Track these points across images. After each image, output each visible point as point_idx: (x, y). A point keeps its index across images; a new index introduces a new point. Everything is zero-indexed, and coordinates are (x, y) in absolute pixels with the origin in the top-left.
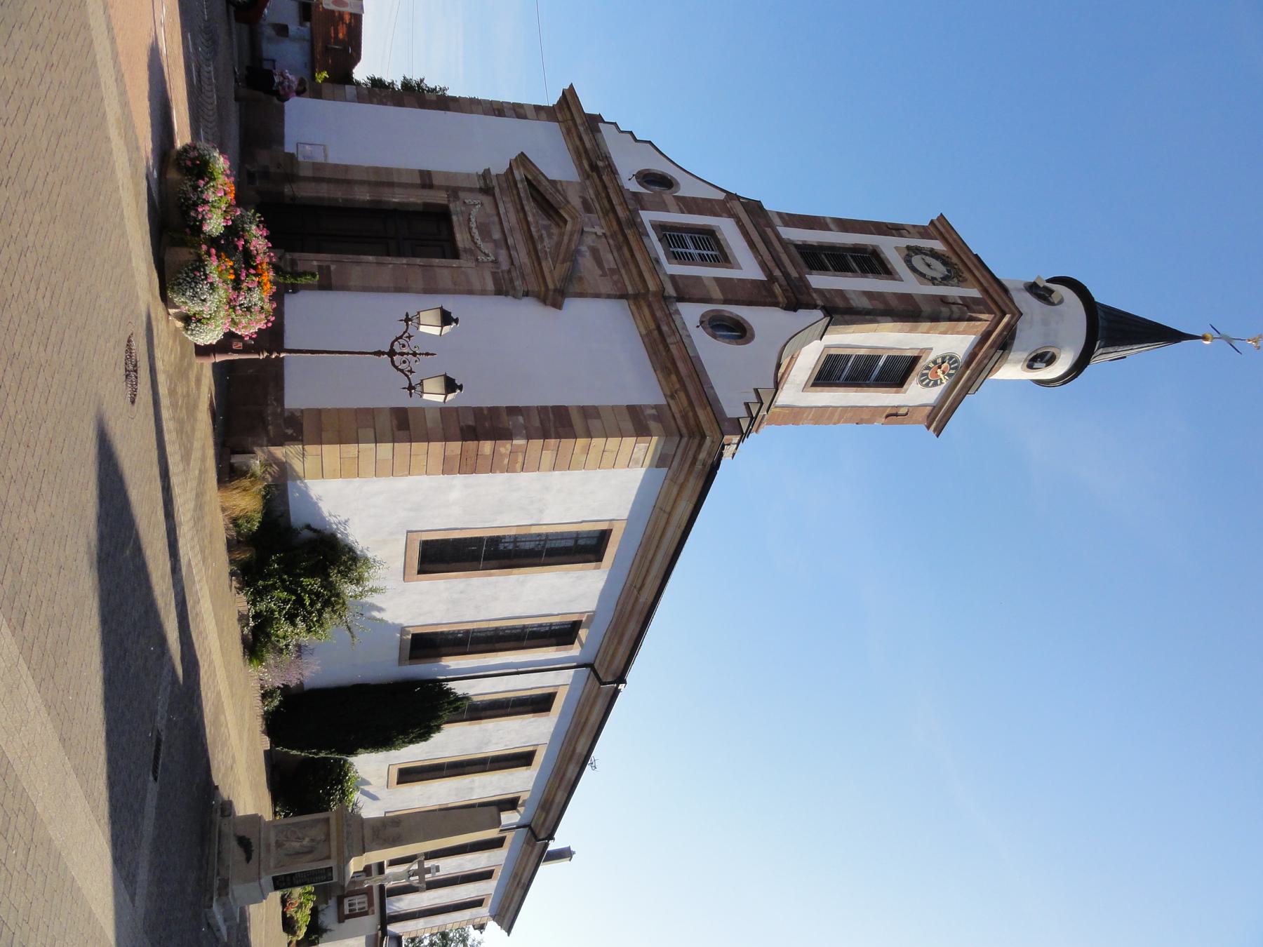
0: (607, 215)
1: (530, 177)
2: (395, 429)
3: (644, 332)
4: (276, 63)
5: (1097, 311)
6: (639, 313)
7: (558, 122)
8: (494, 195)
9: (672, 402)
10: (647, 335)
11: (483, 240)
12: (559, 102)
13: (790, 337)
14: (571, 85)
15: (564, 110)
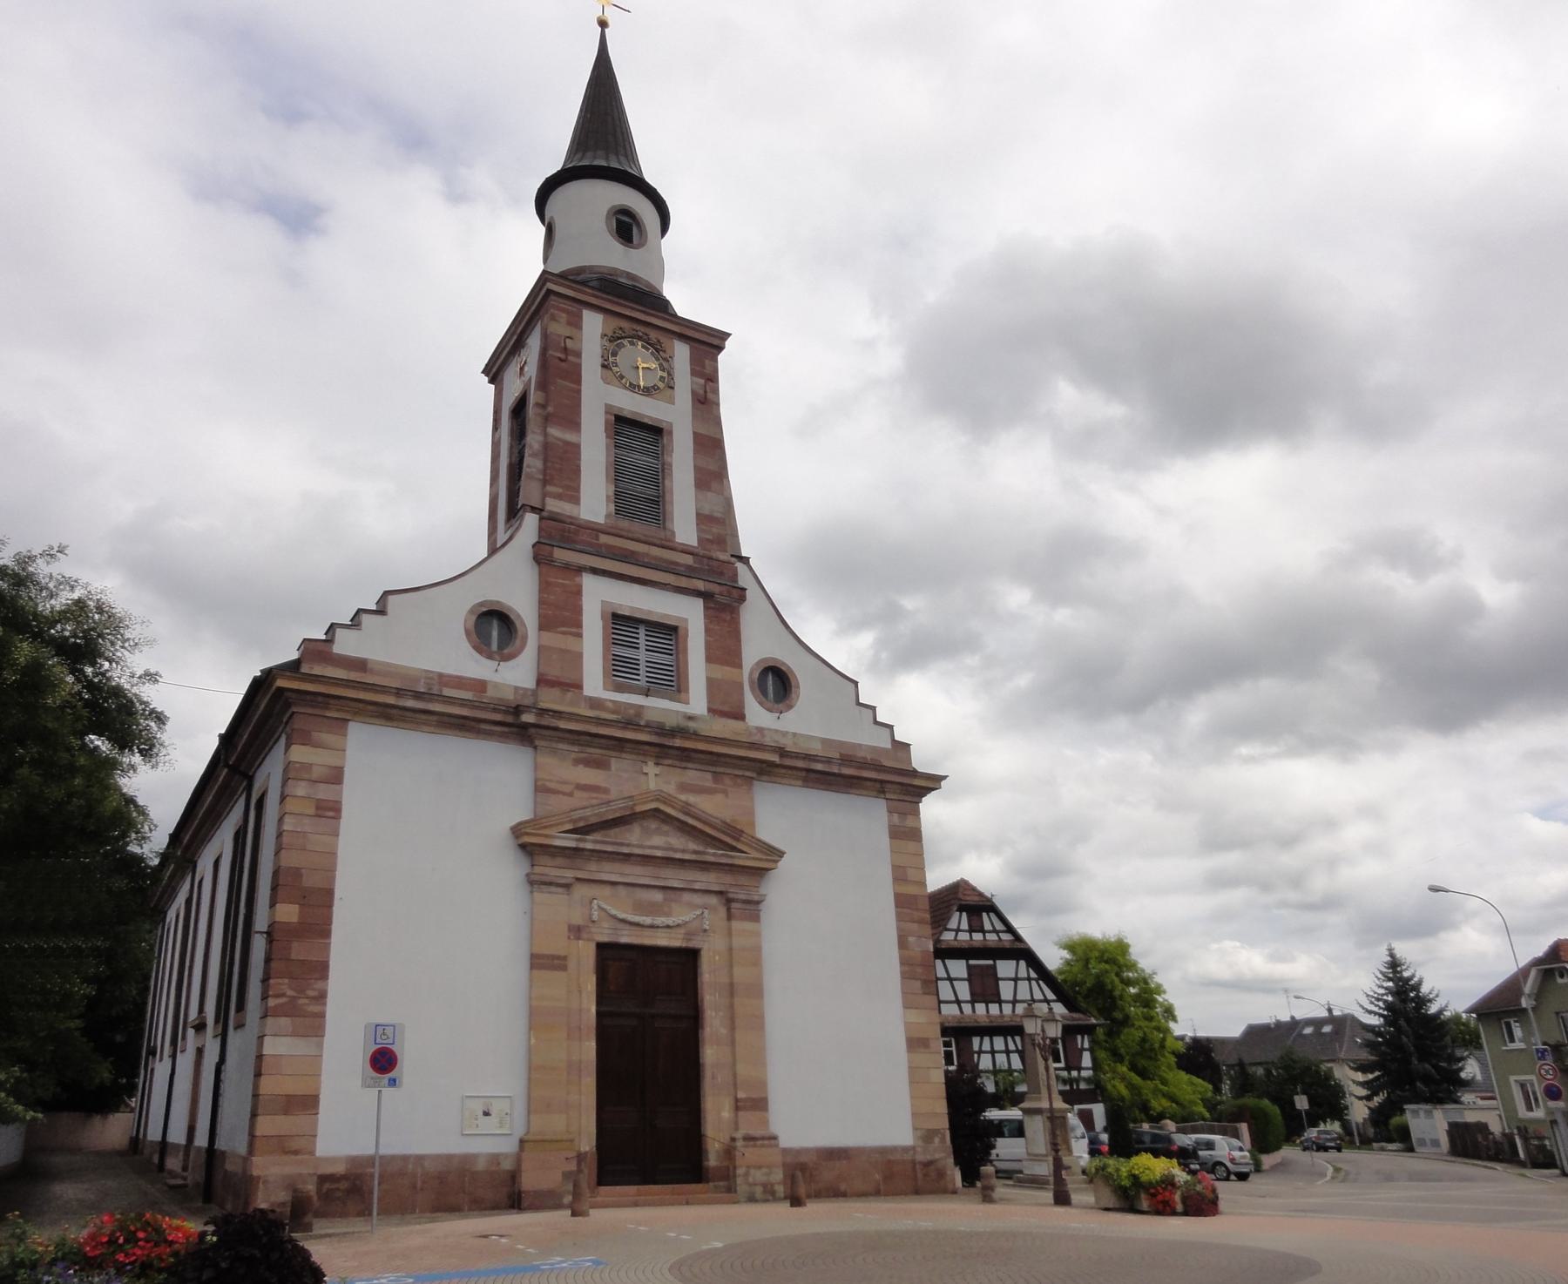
1: (569, 827)
3: (800, 783)
7: (349, 720)
8: (578, 879)
11: (668, 915)
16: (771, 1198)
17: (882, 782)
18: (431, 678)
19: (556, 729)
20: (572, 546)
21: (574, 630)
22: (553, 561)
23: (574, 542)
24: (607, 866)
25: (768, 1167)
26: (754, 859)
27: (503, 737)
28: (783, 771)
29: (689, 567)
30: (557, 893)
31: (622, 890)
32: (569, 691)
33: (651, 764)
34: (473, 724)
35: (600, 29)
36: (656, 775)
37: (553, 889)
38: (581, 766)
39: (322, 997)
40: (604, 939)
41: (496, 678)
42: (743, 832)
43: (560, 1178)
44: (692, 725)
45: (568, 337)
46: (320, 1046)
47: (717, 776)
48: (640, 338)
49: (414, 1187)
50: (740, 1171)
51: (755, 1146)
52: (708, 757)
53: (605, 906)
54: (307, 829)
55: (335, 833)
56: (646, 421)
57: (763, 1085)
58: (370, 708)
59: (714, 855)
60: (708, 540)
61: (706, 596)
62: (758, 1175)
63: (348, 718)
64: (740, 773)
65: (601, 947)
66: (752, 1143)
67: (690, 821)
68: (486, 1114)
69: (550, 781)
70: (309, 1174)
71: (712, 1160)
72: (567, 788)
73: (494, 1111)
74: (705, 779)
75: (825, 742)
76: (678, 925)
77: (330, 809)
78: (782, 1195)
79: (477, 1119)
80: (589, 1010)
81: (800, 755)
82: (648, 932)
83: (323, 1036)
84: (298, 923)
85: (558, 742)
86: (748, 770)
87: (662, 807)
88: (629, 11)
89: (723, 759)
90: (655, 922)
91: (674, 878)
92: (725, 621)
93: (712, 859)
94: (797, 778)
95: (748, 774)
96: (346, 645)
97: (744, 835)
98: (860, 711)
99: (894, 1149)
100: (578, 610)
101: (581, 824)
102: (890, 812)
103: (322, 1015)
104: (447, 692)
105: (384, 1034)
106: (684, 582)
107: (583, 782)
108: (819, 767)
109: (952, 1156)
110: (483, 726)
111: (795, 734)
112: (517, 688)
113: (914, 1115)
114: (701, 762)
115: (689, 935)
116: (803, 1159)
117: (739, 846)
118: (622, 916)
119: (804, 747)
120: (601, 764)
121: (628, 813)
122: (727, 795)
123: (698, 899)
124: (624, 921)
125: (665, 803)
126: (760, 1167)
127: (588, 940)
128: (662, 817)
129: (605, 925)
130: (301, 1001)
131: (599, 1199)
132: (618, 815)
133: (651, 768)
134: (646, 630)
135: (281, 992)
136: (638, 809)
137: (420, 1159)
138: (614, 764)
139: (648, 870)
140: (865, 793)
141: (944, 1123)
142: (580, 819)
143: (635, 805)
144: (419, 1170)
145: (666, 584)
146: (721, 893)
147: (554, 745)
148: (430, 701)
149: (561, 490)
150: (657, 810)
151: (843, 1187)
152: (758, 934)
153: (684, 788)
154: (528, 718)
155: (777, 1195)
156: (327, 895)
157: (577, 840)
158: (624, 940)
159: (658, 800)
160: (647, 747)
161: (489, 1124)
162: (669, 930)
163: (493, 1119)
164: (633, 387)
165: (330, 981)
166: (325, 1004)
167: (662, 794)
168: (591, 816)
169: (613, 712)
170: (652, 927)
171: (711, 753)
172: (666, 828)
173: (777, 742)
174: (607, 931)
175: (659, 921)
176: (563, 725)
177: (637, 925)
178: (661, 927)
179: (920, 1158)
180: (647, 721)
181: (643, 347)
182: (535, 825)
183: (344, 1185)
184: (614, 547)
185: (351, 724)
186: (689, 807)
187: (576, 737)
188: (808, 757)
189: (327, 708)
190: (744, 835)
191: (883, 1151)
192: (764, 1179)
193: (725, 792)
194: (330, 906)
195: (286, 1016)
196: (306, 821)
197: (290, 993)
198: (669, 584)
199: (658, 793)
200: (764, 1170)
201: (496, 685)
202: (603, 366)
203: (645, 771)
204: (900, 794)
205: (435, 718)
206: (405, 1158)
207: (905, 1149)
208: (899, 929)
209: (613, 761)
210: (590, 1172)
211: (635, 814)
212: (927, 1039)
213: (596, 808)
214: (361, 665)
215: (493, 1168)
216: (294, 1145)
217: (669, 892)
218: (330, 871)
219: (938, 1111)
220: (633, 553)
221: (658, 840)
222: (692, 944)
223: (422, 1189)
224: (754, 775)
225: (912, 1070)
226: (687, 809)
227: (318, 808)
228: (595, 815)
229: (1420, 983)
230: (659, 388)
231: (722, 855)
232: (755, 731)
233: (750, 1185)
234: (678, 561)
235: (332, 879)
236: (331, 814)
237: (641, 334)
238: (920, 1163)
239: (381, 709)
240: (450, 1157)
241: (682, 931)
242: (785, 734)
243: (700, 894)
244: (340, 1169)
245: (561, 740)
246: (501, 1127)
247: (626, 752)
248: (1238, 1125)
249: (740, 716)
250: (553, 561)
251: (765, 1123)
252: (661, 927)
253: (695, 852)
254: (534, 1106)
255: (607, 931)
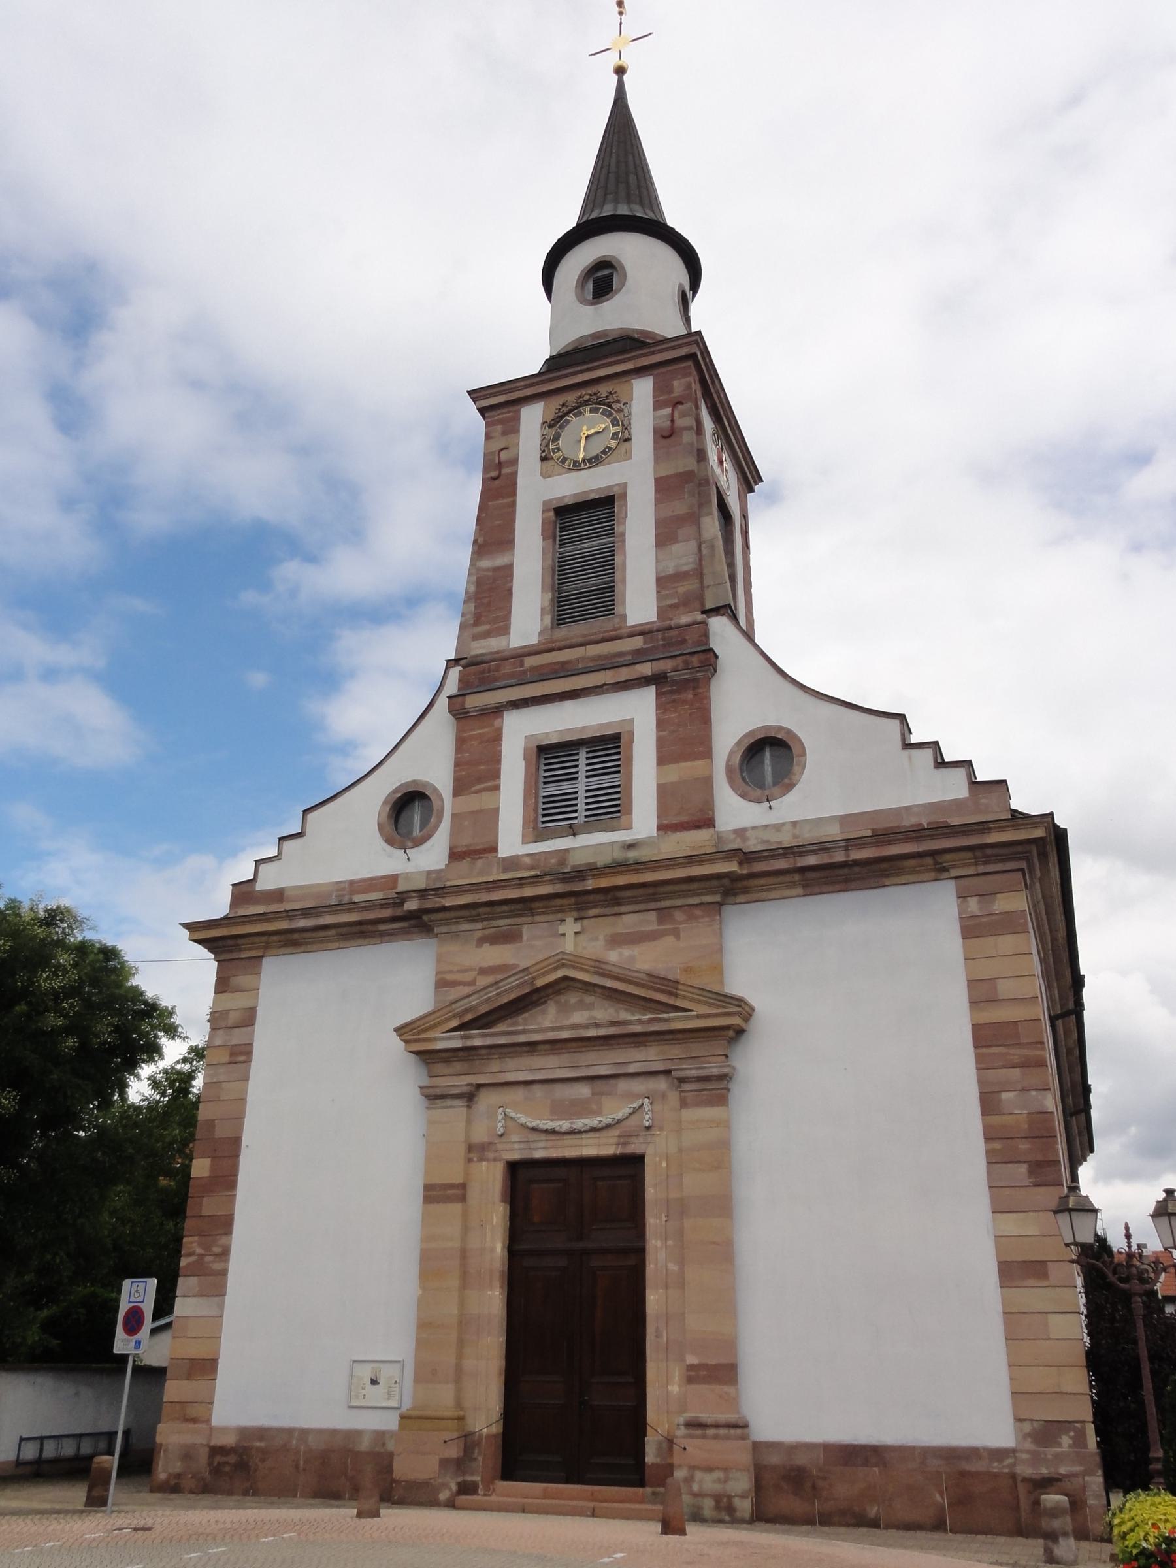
0: (531, 909)
1: (455, 1023)
2: (1046, 1283)
3: (800, 891)
4: (24, 1437)
5: (592, 219)
6: (758, 891)
7: (262, 957)
8: (479, 1086)
9: (954, 873)
10: (804, 886)
11: (598, 1113)
12: (211, 950)
13: (778, 677)
14: (187, 926)
15: (238, 945)
16: (727, 1518)
17: (933, 854)
18: (343, 889)
19: (444, 909)
20: (492, 686)
21: (490, 784)
22: (468, 712)
23: (495, 680)
24: (511, 1063)
25: (726, 1470)
26: (698, 1017)
27: (405, 934)
28: (762, 881)
29: (637, 652)
30: (454, 1107)
31: (538, 1091)
32: (480, 858)
33: (570, 920)
34: (370, 928)
35: (616, 78)
36: (576, 933)
37: (449, 1102)
38: (486, 946)
39: (225, 1253)
40: (515, 1156)
41: (409, 868)
42: (677, 982)
43: (437, 1467)
44: (632, 855)
45: (502, 449)
46: (221, 1307)
47: (664, 914)
48: (586, 403)
49: (297, 1467)
50: (679, 1474)
51: (704, 1437)
52: (641, 891)
53: (513, 1114)
54: (222, 1078)
55: (246, 1079)
56: (593, 496)
57: (730, 1344)
58: (275, 938)
59: (640, 1022)
60: (671, 606)
61: (656, 680)
62: (707, 1482)
63: (260, 954)
64: (696, 900)
65: (514, 1168)
66: (699, 1432)
67: (609, 983)
68: (374, 1382)
69: (451, 972)
70: (201, 1444)
71: (651, 1457)
72: (468, 977)
73: (382, 1381)
74: (648, 921)
75: (844, 820)
76: (608, 1126)
77: (241, 1053)
78: (747, 1516)
79: (363, 1389)
80: (493, 1250)
81: (776, 852)
82: (570, 1140)
83: (225, 1295)
84: (210, 1177)
85: (457, 923)
86: (707, 894)
87: (571, 973)
88: (650, 34)
89: (662, 889)
90: (574, 1126)
91: (600, 1062)
92: (684, 702)
93: (638, 1028)
94: (793, 885)
95: (708, 899)
96: (268, 881)
97: (680, 987)
98: (910, 758)
99: (973, 1453)
100: (496, 759)
101: (469, 1017)
102: (962, 896)
103: (224, 1273)
104: (357, 898)
105: (137, 1291)
106: (624, 674)
107: (485, 964)
108: (812, 860)
109: (1100, 1472)
110: (382, 927)
111: (794, 824)
112: (429, 873)
113: (1017, 1394)
114: (635, 900)
115: (625, 1138)
116: (801, 1460)
117: (679, 1003)
118: (534, 1123)
119: (808, 836)
120: (510, 937)
121: (527, 991)
122: (677, 937)
123: (638, 1086)
124: (534, 1129)
125: (574, 968)
126: (709, 1469)
127: (495, 1160)
128: (580, 986)
129: (515, 1138)
130: (208, 1259)
131: (494, 1498)
132: (513, 996)
133: (570, 926)
134: (588, 752)
135: (191, 1250)
136: (540, 983)
137: (304, 1432)
138: (526, 931)
139: (564, 1059)
140: (911, 878)
141: (1084, 1412)
142: (466, 1011)
143: (534, 979)
144: (302, 1448)
145: (601, 686)
146: (667, 1072)
147: (454, 928)
148: (317, 915)
149: (487, 627)
150: (566, 978)
151: (873, 1511)
152: (726, 1125)
153: (616, 941)
154: (412, 905)
155: (738, 1514)
156: (235, 1143)
157: (463, 1037)
158: (539, 1154)
159: (563, 965)
160: (559, 902)
161: (376, 1395)
162: (597, 1135)
163: (380, 1389)
164: (577, 466)
165: (233, 1236)
166: (227, 1261)
167: (566, 957)
168: (478, 1005)
169: (532, 868)
170: (572, 1132)
171: (643, 885)
172: (589, 999)
173: (768, 842)
174: (517, 1146)
175: (579, 1124)
176: (449, 902)
177: (553, 1132)
178: (585, 1132)
179: (1025, 1470)
180: (574, 866)
181: (591, 411)
182: (412, 1030)
183: (232, 1459)
184: (542, 666)
185: (265, 961)
186: (603, 966)
187: (472, 911)
188: (823, 847)
189: (240, 950)
190: (680, 987)
191: (951, 1454)
192: (718, 1488)
193: (676, 933)
194: (236, 1155)
195: (194, 1276)
196: (222, 1070)
197: (199, 1251)
198: (605, 684)
199: (560, 957)
200: (718, 1474)
201: (407, 876)
202: (543, 459)
203: (561, 932)
204: (976, 864)
205: (333, 932)
206: (290, 1431)
207: (998, 1454)
208: (981, 1082)
209: (525, 929)
210: (486, 1459)
211: (538, 990)
212: (1044, 1263)
213: (482, 993)
214: (278, 895)
215: (377, 1449)
216: (192, 1411)
217: (599, 1083)
218: (238, 1119)
219: (1068, 1388)
220: (563, 664)
221: (578, 1017)
222: (633, 1148)
223: (304, 1470)
224: (717, 898)
225: (1012, 1317)
226: (599, 967)
227: (232, 1054)
228: (484, 1002)
229: (149, 1085)
230: (610, 448)
231: (651, 1020)
232: (732, 836)
233: (695, 1495)
234: (623, 649)
235: (240, 1127)
236: (242, 1058)
237: (586, 398)
238: (1025, 1480)
239: (283, 937)
240: (334, 1432)
241: (615, 1132)
242: (778, 827)
243: (641, 1079)
244: (230, 1440)
245: (459, 920)
246: (388, 1399)
247: (538, 914)
248: (658, 1460)
249: (706, 821)
250: (468, 712)
251: (734, 1402)
252: (585, 1132)
253: (613, 1024)
254: (425, 1373)
255: (517, 1146)
